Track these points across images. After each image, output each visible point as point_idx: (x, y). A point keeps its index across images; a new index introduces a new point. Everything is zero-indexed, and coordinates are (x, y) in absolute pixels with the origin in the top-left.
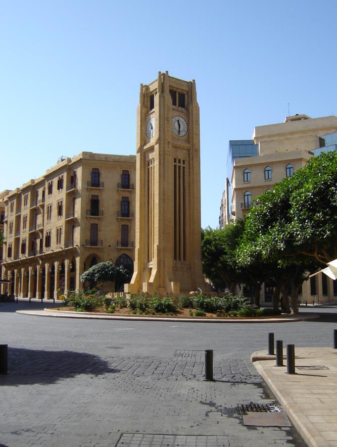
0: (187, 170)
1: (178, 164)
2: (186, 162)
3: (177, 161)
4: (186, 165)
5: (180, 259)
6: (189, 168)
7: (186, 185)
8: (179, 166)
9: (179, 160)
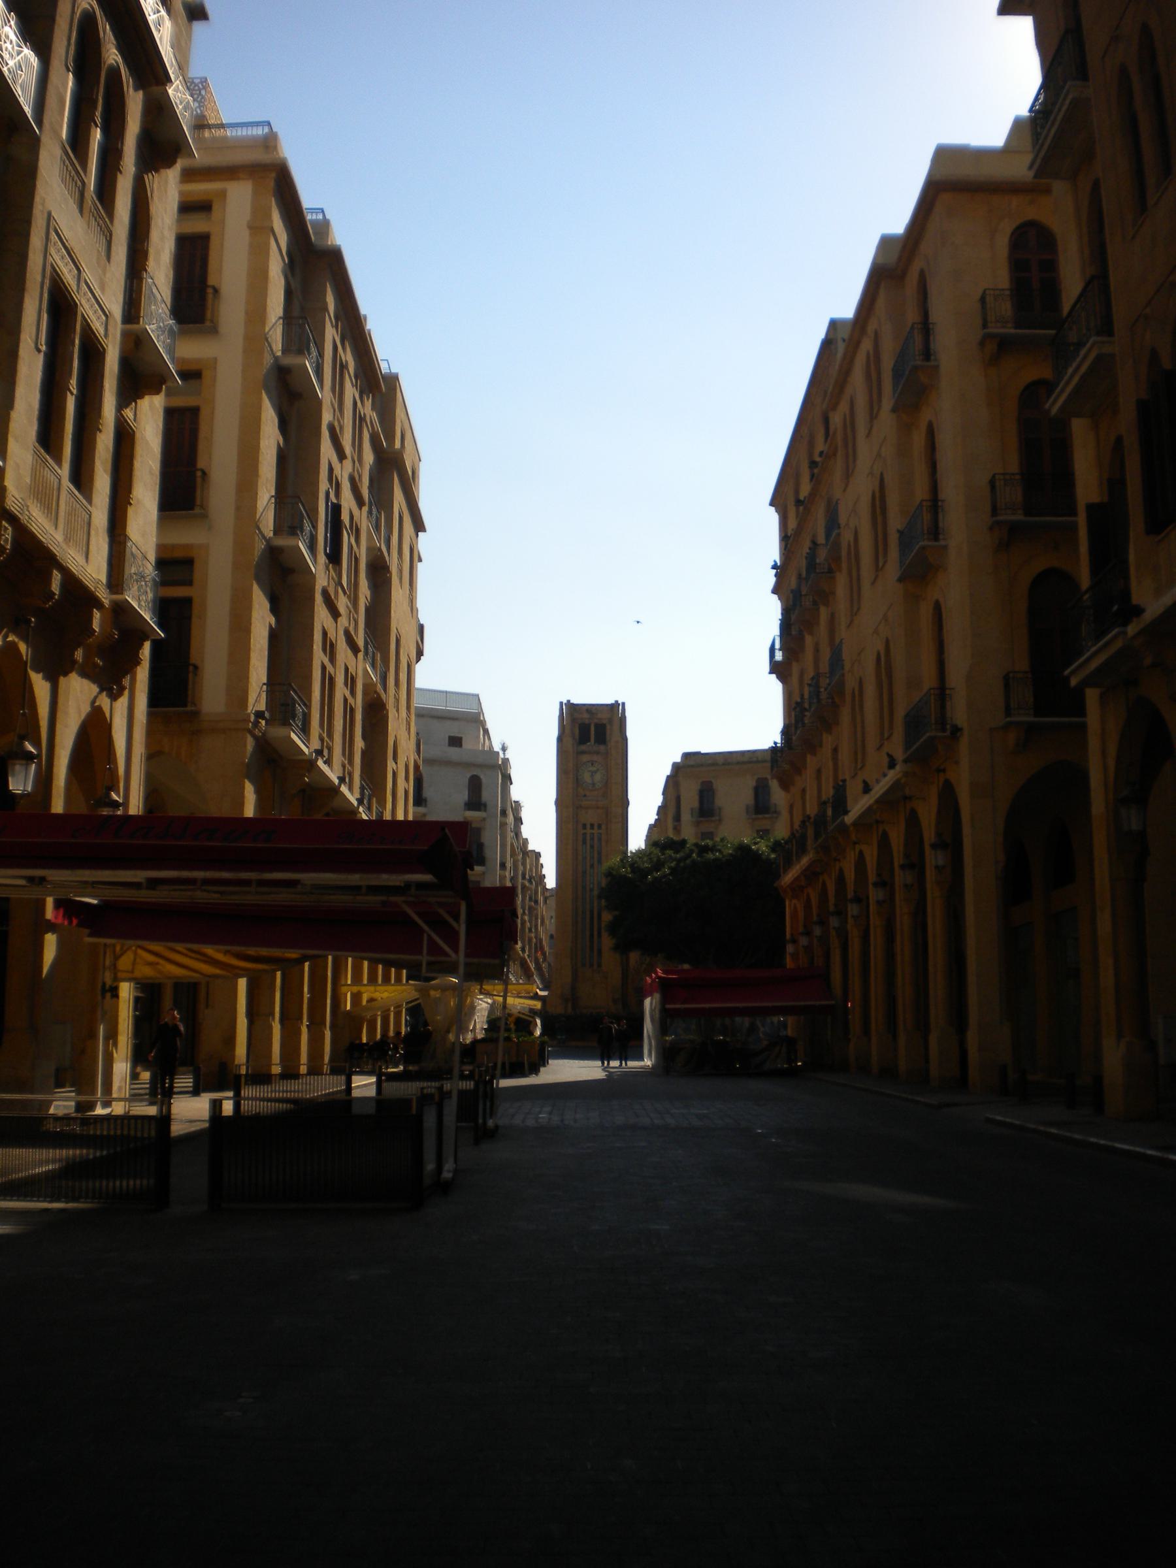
2: (603, 827)
3: (588, 826)
9: (592, 826)
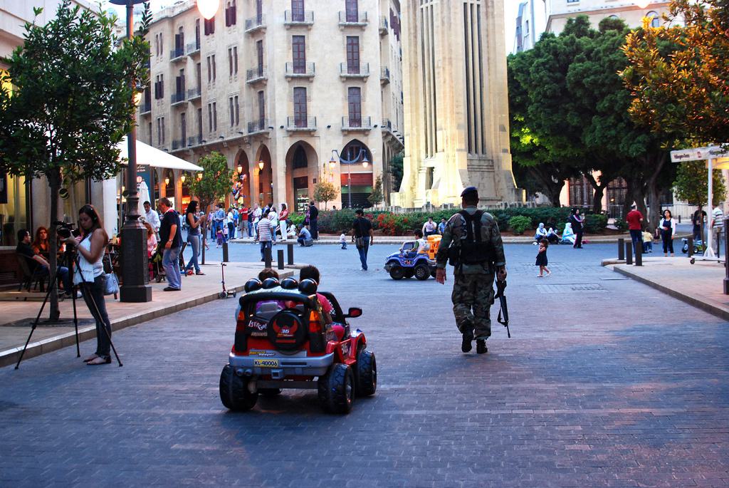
0: (482, 10)
5: (472, 5)
6: (487, 6)
7: (483, 33)
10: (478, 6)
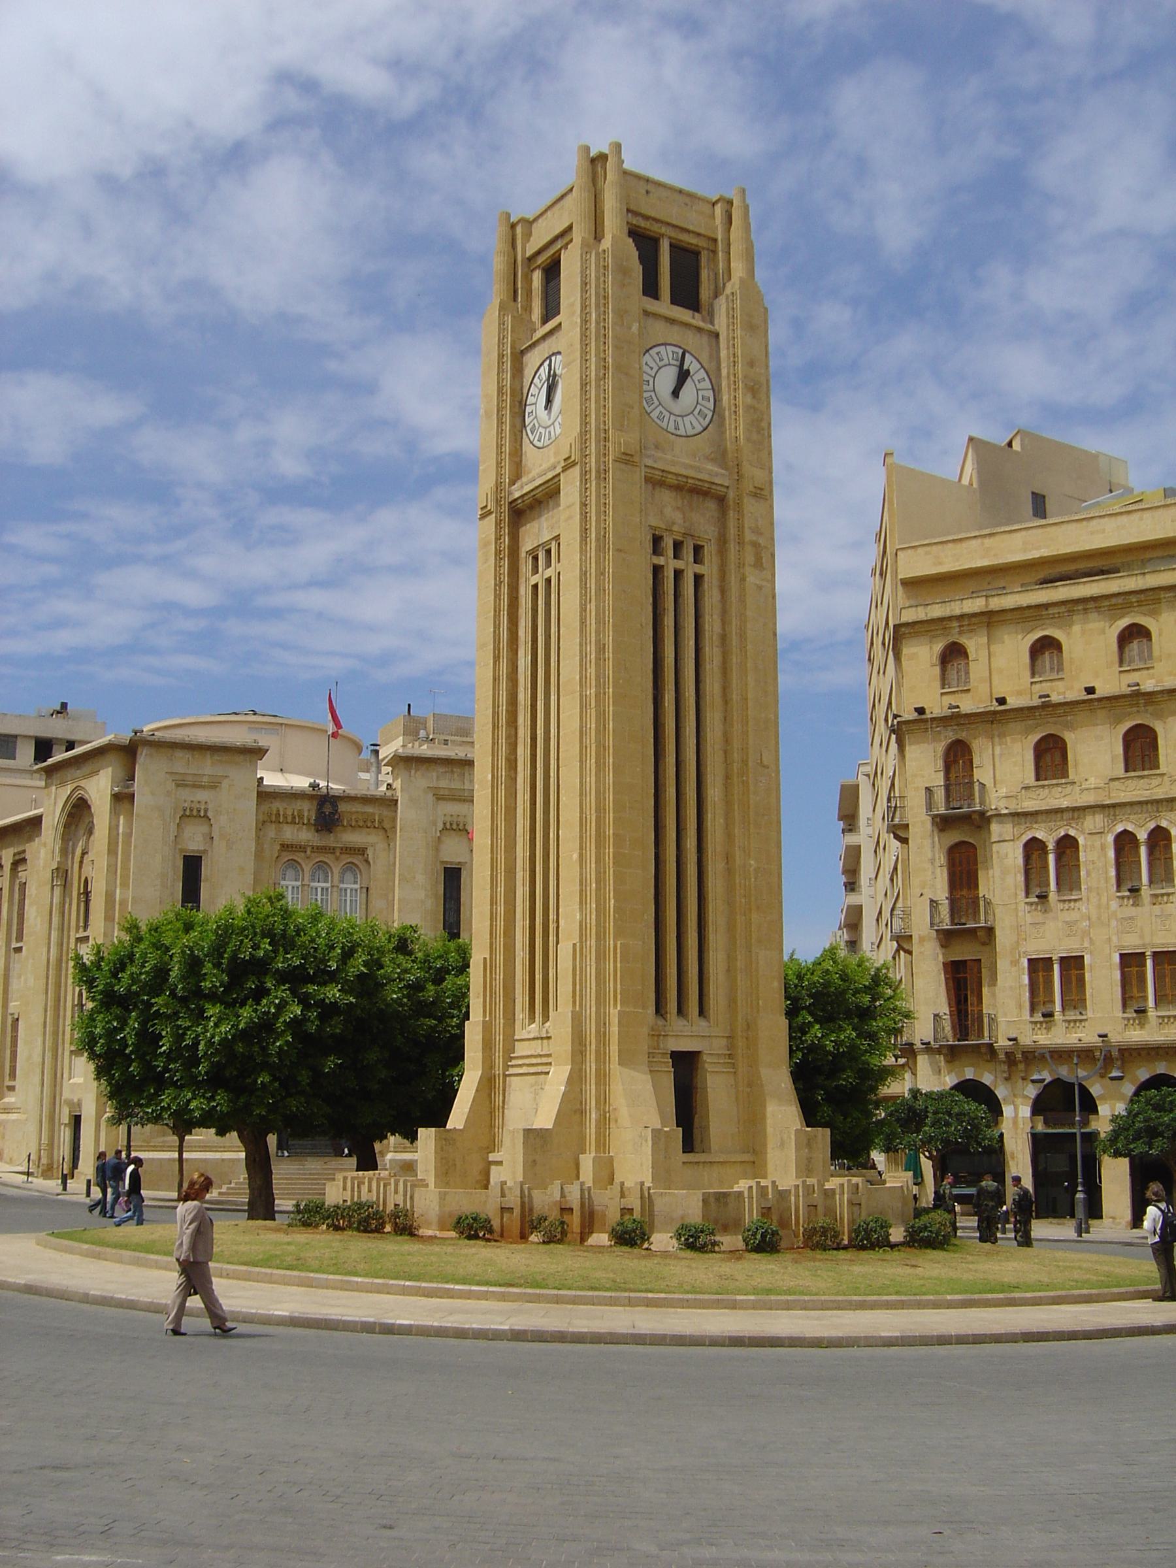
1: (670, 564)
2: (710, 551)
4: (708, 569)
8: (678, 574)
10: (698, 578)
